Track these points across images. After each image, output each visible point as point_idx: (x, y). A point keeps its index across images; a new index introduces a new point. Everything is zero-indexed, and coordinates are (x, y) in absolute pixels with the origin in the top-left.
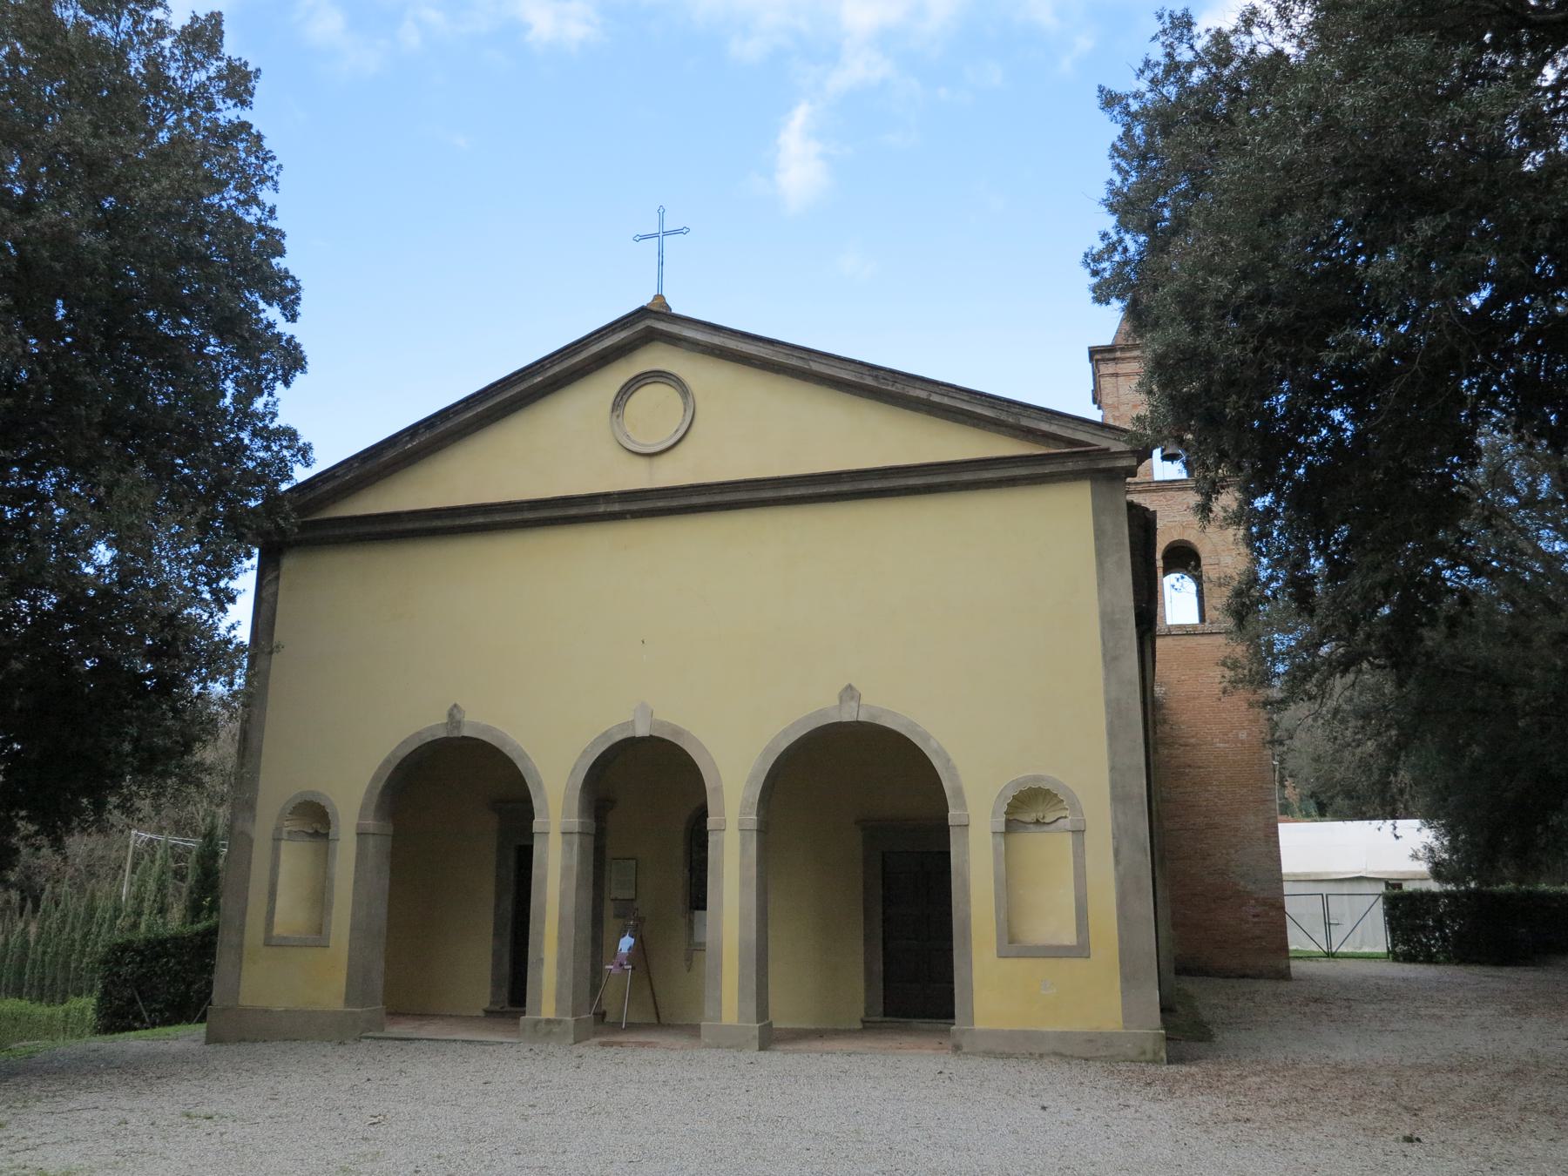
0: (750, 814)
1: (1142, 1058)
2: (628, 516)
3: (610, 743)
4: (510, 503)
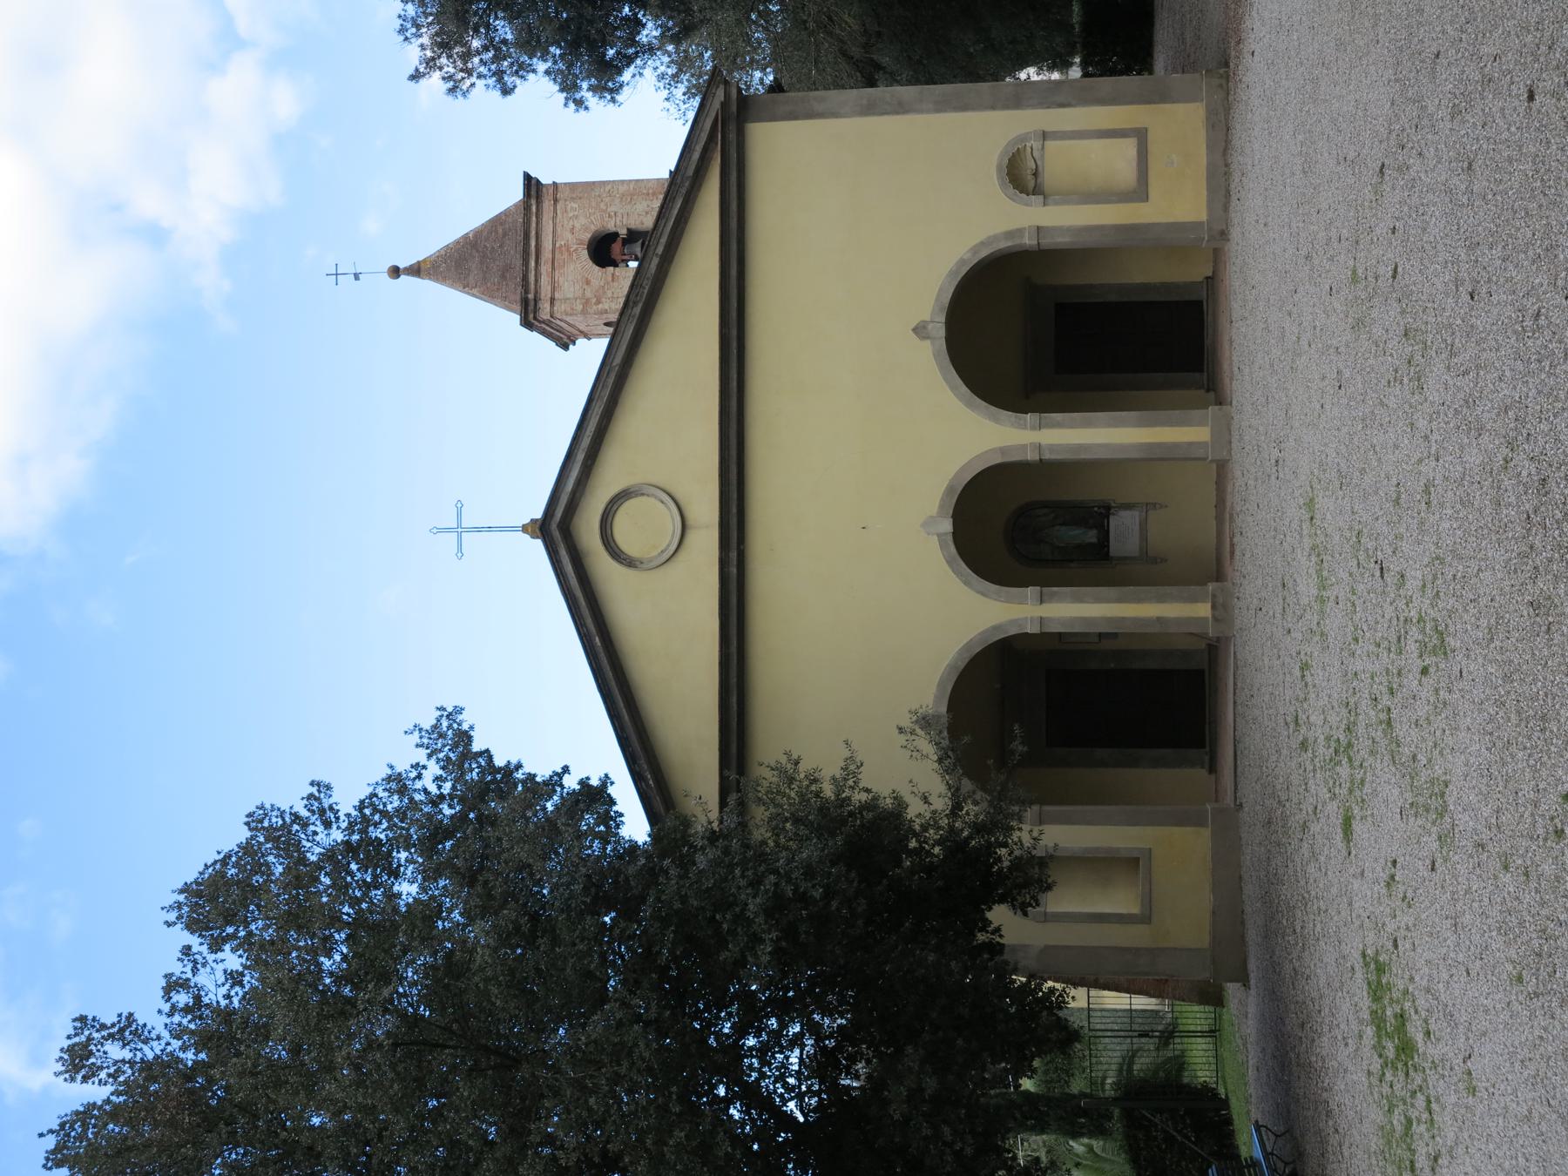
0: (1025, 420)
4: (721, 664)
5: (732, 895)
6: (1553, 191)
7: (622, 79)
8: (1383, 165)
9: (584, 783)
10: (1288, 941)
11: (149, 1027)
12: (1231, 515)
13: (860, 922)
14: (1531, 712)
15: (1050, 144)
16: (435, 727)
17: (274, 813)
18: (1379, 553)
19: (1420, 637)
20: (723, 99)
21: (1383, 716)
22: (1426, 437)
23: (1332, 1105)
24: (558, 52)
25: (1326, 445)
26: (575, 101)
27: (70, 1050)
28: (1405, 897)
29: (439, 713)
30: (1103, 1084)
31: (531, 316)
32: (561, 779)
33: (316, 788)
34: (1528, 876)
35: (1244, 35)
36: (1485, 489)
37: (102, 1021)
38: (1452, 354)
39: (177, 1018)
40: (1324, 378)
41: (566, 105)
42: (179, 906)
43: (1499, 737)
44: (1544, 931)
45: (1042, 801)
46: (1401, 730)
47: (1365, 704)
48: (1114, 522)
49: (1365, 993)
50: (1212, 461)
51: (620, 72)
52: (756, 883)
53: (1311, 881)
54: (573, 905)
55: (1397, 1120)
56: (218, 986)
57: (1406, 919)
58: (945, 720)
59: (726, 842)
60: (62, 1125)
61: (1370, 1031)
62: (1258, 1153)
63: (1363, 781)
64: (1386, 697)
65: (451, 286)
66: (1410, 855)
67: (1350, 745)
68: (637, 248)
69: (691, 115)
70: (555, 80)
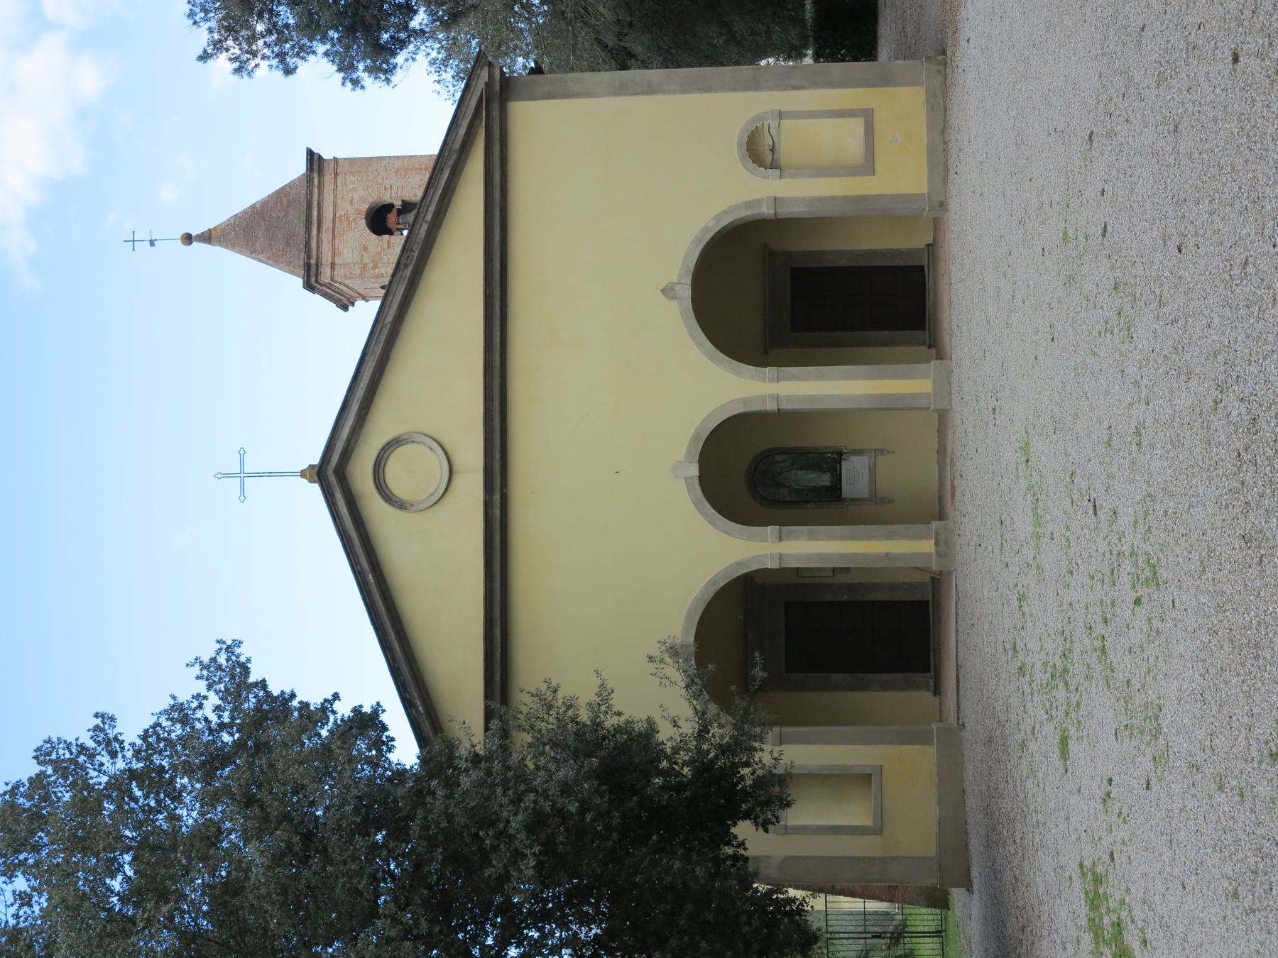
0: (765, 373)
1: (943, 72)
2: (505, 491)
5: (495, 813)
6: (1259, 145)
7: (395, 61)
8: (1092, 133)
9: (357, 711)
10: (1009, 851)
12: (952, 460)
13: (615, 836)
14: (1244, 641)
15: (785, 122)
16: (214, 660)
17: (61, 746)
18: (1092, 492)
19: (1133, 570)
20: (487, 80)
24: (336, 35)
25: (1040, 393)
29: (218, 646)
32: (332, 705)
33: (100, 719)
34: (1243, 797)
35: (960, 25)
36: (1195, 430)
38: (1161, 304)
40: (1037, 332)
41: (343, 84)
43: (1212, 664)
44: (1260, 850)
45: (783, 723)
46: (1113, 657)
48: (845, 466)
49: (1083, 902)
50: (934, 410)
51: (394, 54)
52: (517, 801)
53: (1030, 795)
54: (344, 825)
56: (7, 906)
57: (1121, 834)
58: (692, 649)
59: (487, 764)
61: (1087, 938)
63: (1078, 704)
65: (240, 252)
66: (1125, 774)
67: (1066, 671)
68: (410, 217)
69: (458, 96)
70: (333, 61)
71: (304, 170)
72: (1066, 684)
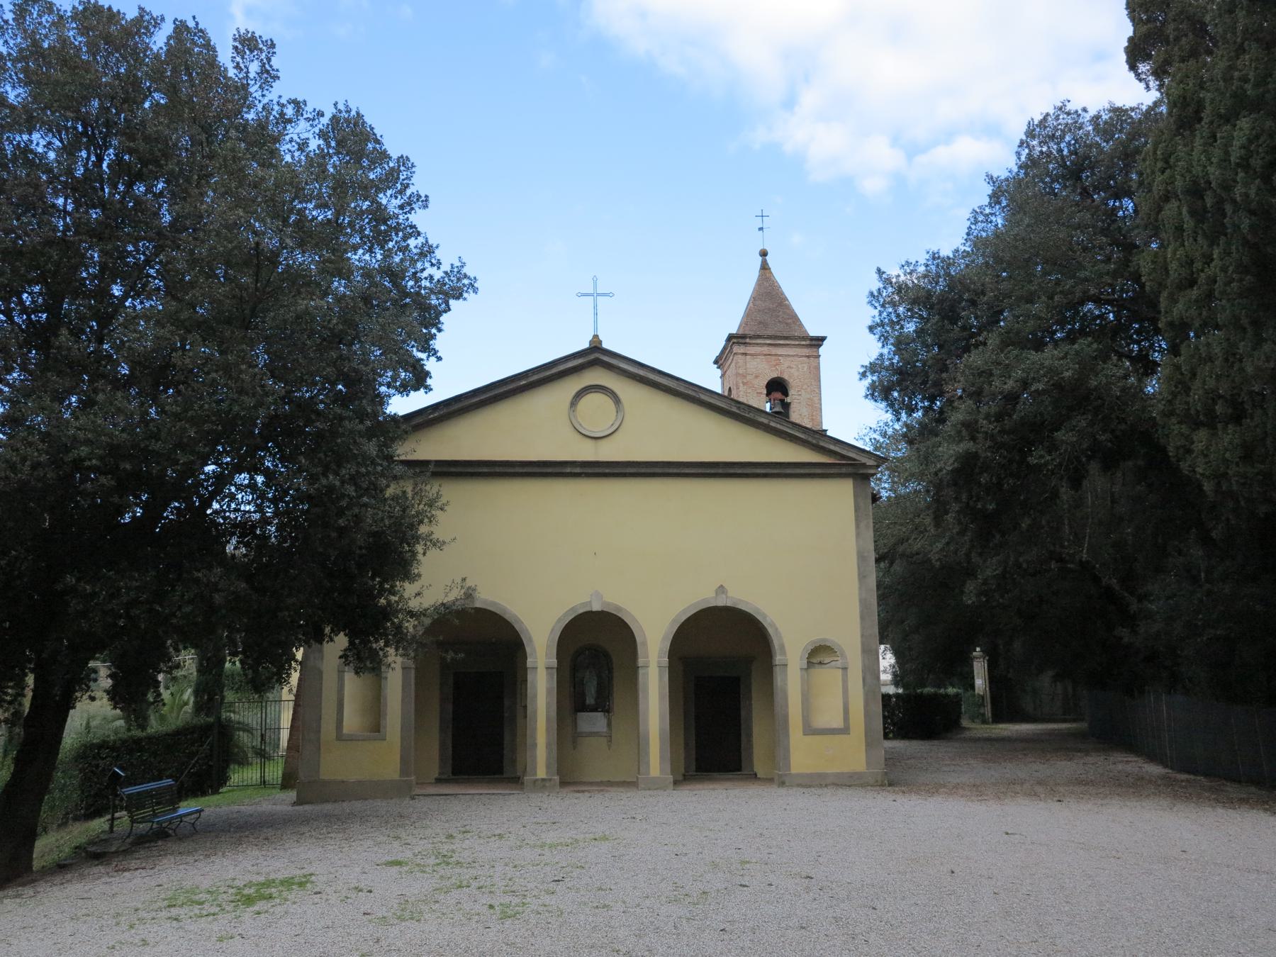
3: (576, 614)
8: (812, 878)
9: (428, 374)
11: (270, 89)
12: (602, 791)
16: (466, 276)
21: (465, 883)
22: (639, 905)
23: (213, 858)
26: (865, 372)
27: (253, 38)
28: (348, 898)
30: (230, 711)
31: (735, 341)
37: (272, 58)
39: (276, 108)
40: (684, 845)
41: (863, 366)
42: (348, 111)
46: (455, 894)
47: (473, 872)
48: (599, 715)
55: (203, 896)
60: (201, 31)
61: (262, 879)
62: (181, 811)
63: (424, 872)
64: (477, 885)
67: (448, 864)
69: (860, 444)
71: (812, 334)
72: (438, 864)
